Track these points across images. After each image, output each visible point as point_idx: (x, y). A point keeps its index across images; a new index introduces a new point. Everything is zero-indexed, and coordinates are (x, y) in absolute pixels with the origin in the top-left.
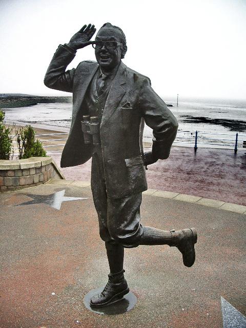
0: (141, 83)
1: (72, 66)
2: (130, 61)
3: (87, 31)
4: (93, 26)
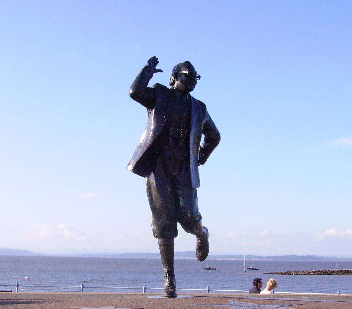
0: (201, 106)
1: (151, 84)
2: (196, 94)
3: (154, 61)
4: (157, 59)
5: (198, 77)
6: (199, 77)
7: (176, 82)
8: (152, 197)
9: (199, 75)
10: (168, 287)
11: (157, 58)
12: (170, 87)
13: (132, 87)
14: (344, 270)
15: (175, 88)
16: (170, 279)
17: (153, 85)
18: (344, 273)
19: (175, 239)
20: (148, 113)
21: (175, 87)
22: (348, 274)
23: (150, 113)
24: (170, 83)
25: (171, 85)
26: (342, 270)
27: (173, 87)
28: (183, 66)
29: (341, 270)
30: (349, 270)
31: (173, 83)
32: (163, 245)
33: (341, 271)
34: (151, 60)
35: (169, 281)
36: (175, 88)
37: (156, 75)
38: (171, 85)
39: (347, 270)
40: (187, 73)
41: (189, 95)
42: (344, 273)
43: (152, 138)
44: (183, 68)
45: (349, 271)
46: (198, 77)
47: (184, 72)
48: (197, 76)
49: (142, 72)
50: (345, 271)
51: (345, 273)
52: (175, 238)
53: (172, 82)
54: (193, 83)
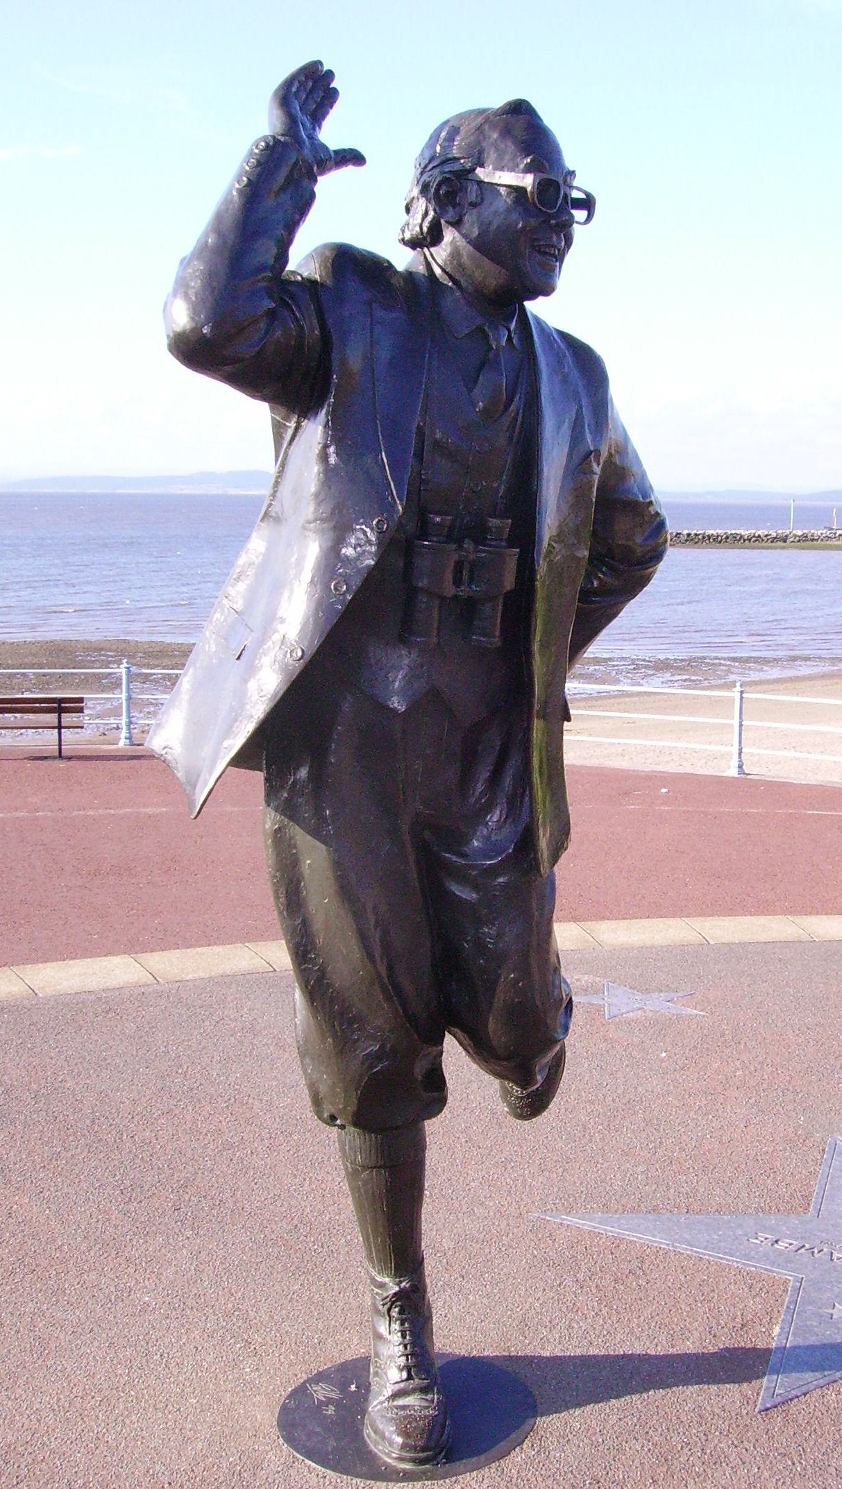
5: (578, 204)
6: (587, 204)
7: (449, 235)
8: (305, 924)
9: (588, 195)
10: (402, 1381)
11: (325, 68)
12: (402, 259)
13: (181, 286)
14: (685, 532)
15: (438, 271)
16: (409, 1347)
17: (311, 256)
18: (687, 541)
19: (433, 1128)
20: (278, 430)
21: (440, 262)
22: (696, 543)
23: (290, 432)
24: (408, 236)
25: (414, 244)
26: (680, 534)
27: (428, 265)
28: (495, 136)
29: (677, 534)
30: (698, 533)
31: (433, 236)
32: (364, 1168)
33: (676, 536)
34: (294, 89)
35: (405, 1347)
36: (443, 270)
37: (328, 186)
38: (414, 244)
39: (695, 532)
40: (529, 189)
41: (519, 316)
42: (687, 541)
43: (317, 610)
44: (497, 149)
45: (700, 537)
46: (578, 204)
47: (507, 178)
48: (576, 194)
49: (247, 186)
50: (689, 535)
51: (688, 543)
52: (427, 1123)
53: (425, 229)
54: (553, 246)
